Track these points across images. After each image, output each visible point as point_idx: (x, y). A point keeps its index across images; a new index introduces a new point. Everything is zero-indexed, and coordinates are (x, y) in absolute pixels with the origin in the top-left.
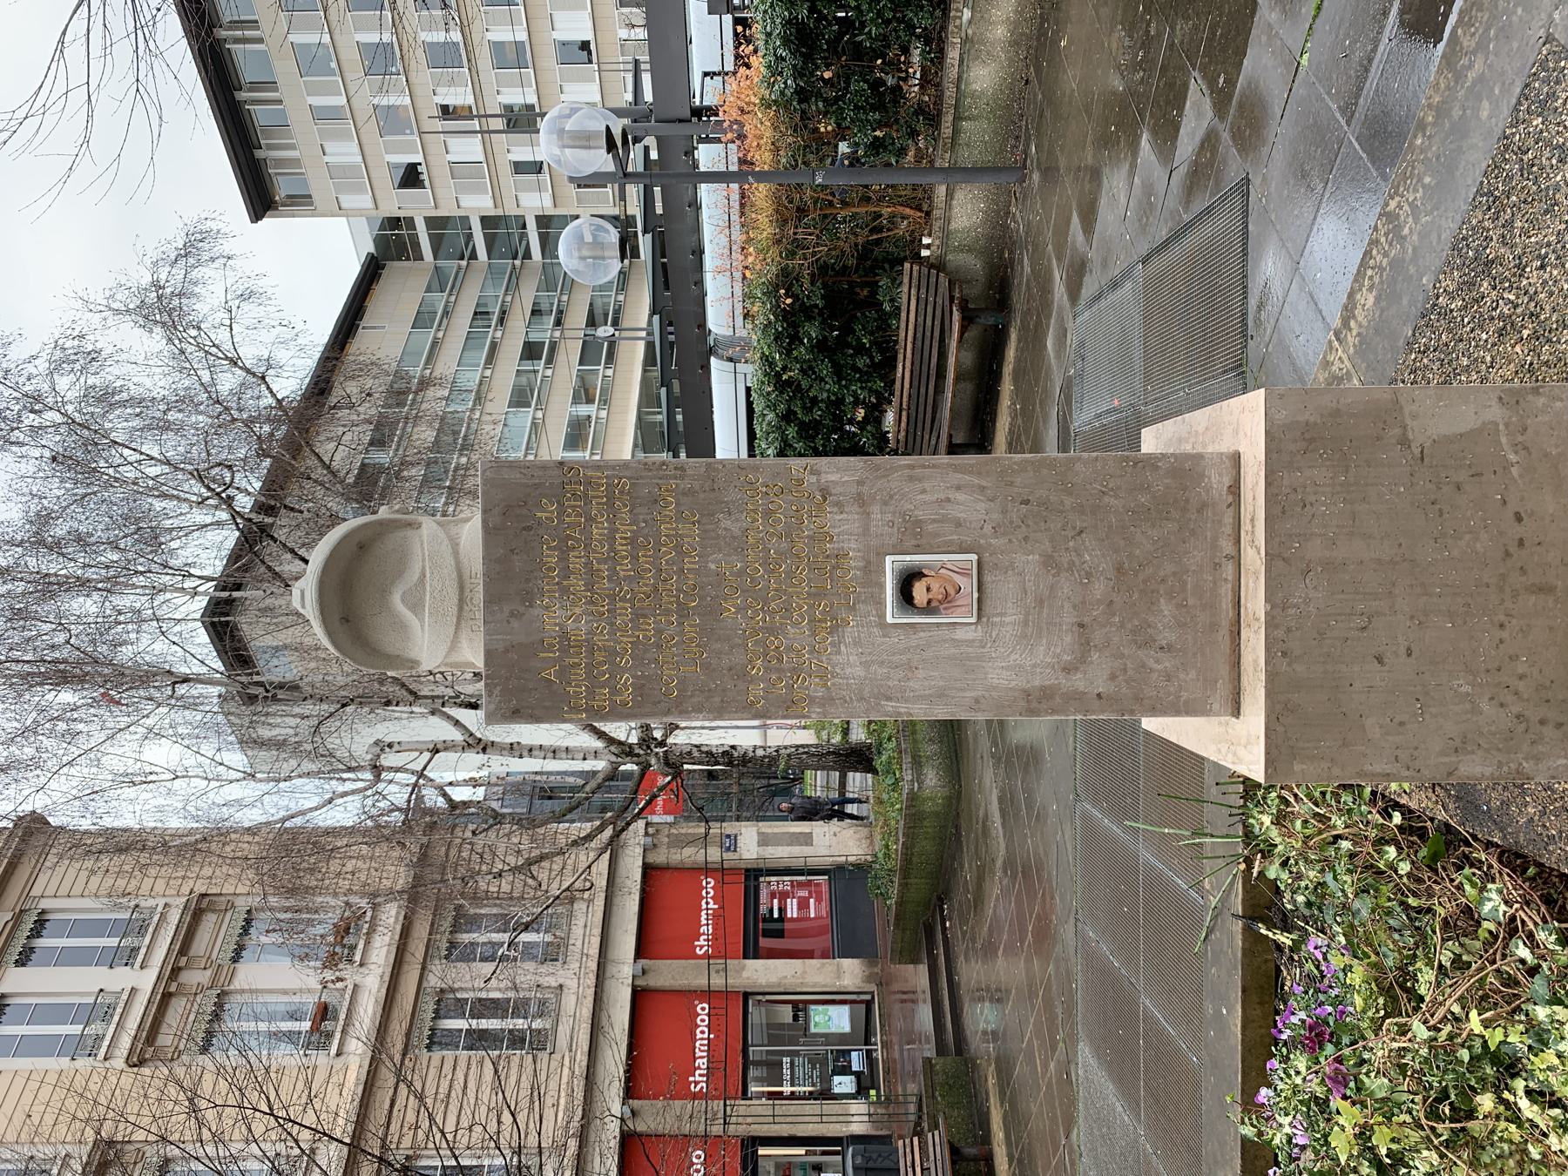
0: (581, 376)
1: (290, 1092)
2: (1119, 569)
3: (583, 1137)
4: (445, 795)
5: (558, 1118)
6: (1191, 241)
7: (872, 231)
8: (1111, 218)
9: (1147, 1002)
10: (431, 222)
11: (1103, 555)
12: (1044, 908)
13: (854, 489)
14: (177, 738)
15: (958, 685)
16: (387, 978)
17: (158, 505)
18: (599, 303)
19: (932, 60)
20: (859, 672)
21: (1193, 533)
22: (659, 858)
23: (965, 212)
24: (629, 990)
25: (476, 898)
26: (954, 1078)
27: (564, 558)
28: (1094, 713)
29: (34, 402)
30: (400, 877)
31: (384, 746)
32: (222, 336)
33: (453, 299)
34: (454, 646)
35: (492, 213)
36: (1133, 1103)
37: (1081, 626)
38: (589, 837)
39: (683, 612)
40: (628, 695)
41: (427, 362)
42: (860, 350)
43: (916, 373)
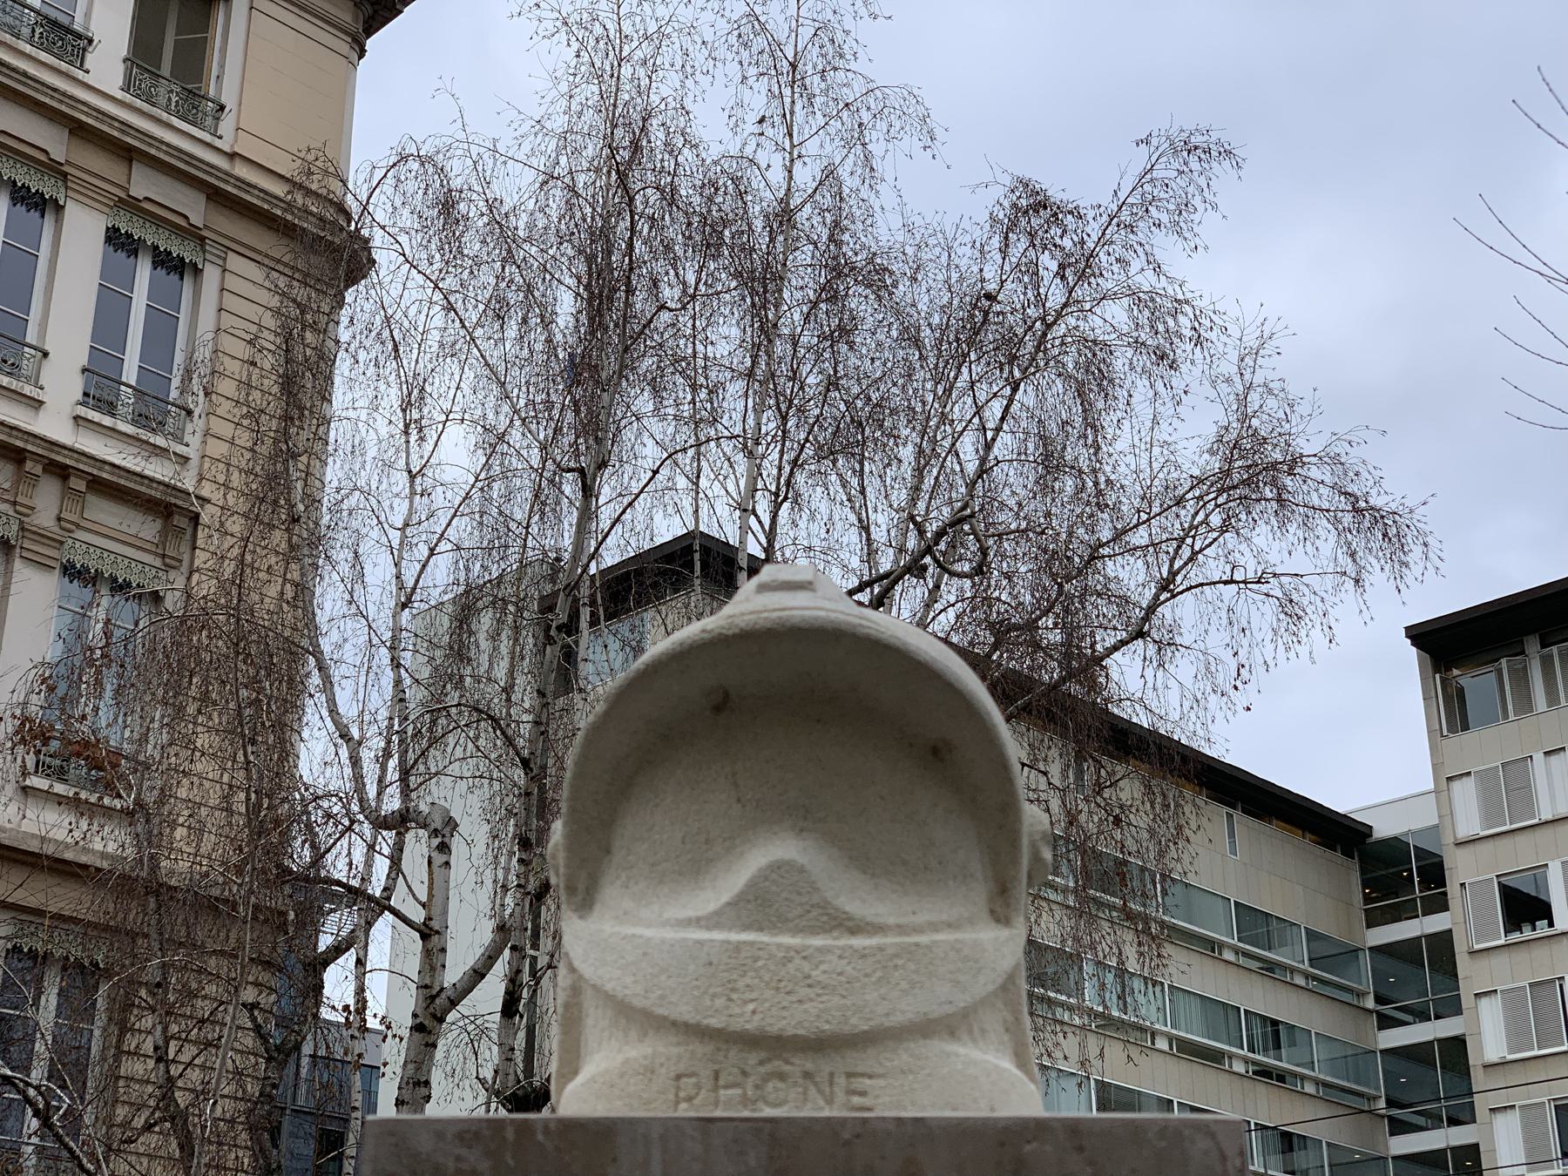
4: (337, 951)
10: (1442, 944)
14: (484, 480)
17: (907, 453)
30: (178, 867)
31: (443, 833)
32: (1211, 566)
33: (1300, 981)
34: (636, 1018)
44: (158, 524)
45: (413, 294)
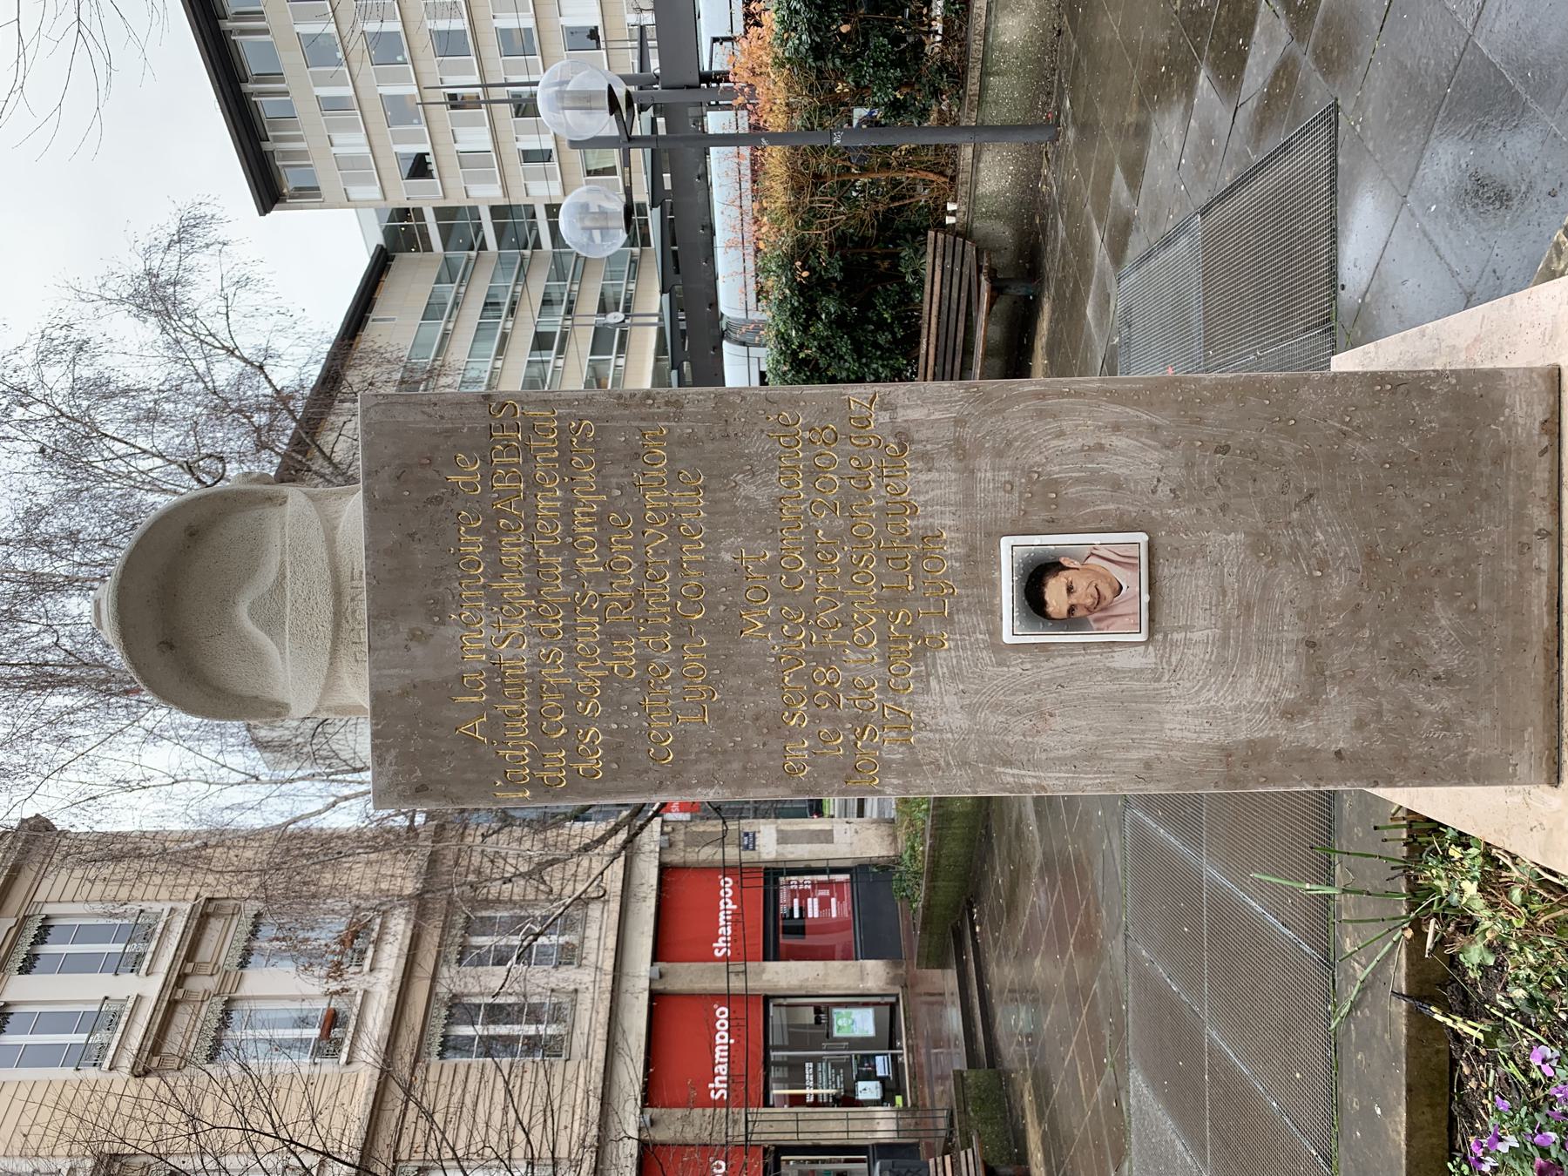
0: (593, 366)
1: (291, 1108)
2: (1370, 555)
3: (600, 1150)
5: (574, 1126)
6: (1260, 185)
7: (893, 199)
8: (1161, 168)
9: (1214, 1034)
10: (440, 213)
11: (1346, 534)
12: (1087, 914)
13: (948, 433)
15: (1118, 740)
16: (398, 984)
18: (610, 293)
19: (956, 12)
20: (960, 720)
21: (1486, 496)
22: (674, 858)
23: (992, 175)
24: (646, 995)
25: (487, 903)
26: (989, 1096)
27: (493, 547)
28: (1330, 781)
29: (22, 396)
32: (218, 325)
33: (463, 290)
35: (502, 202)
36: (1198, 1146)
37: (1311, 644)
38: (602, 840)
39: (682, 628)
40: (595, 762)
41: (437, 355)
42: (881, 325)
43: (942, 348)
44: (212, 920)
45: (53, 791)
